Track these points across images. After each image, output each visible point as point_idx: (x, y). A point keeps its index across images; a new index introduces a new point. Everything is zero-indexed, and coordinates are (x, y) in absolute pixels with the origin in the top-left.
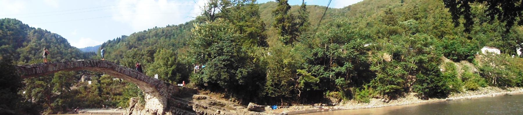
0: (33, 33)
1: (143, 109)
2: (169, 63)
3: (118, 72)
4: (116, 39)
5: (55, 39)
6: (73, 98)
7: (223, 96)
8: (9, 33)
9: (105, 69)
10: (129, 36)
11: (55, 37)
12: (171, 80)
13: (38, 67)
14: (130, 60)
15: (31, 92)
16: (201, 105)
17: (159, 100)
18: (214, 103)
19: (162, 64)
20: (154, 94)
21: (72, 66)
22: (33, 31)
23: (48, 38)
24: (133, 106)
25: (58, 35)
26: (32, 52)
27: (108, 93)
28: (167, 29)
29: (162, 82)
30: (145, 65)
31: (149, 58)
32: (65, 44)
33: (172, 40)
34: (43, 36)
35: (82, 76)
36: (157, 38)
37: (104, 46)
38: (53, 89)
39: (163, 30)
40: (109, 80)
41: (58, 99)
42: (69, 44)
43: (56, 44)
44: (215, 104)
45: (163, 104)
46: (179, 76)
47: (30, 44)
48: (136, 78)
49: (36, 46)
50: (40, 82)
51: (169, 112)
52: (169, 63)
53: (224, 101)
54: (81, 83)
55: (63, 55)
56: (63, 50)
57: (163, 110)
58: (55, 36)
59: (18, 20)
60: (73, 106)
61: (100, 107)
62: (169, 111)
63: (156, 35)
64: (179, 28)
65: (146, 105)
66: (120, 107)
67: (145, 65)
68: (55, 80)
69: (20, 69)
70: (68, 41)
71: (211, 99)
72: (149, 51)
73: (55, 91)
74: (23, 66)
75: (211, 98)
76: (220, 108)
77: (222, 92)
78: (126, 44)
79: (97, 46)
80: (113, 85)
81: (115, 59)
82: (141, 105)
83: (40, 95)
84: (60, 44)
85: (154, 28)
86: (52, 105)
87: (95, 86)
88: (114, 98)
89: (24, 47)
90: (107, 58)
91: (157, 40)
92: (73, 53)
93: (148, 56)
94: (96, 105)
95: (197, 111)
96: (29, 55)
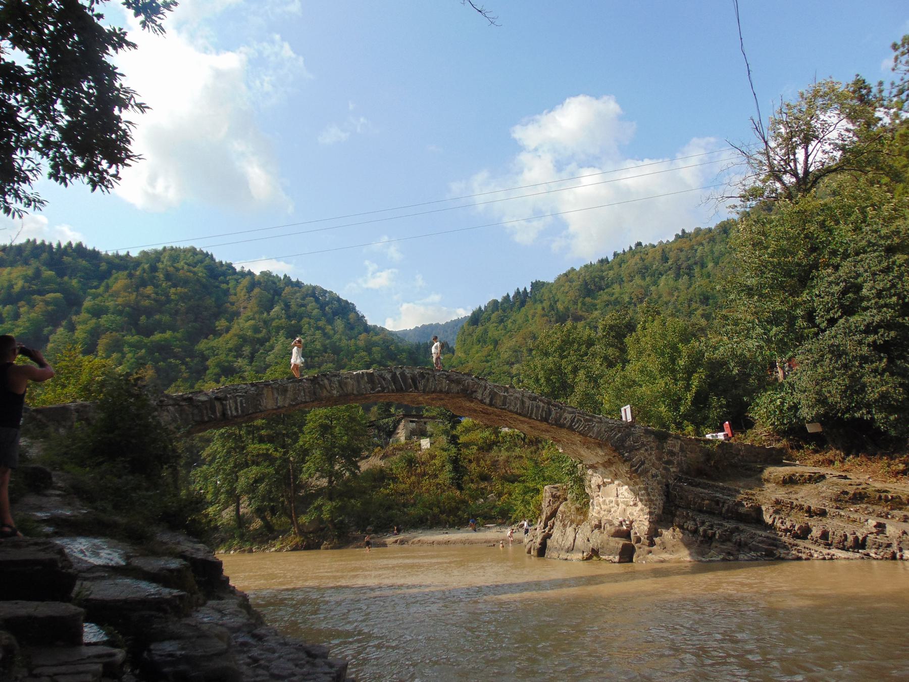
0: (245, 290)
1: (583, 521)
4: (511, 297)
7: (901, 467)
8: (175, 294)
10: (551, 280)
11: (317, 300)
12: (693, 423)
14: (550, 362)
16: (795, 503)
17: (631, 490)
18: (855, 494)
20: (613, 469)
21: (335, 392)
22: (245, 282)
24: (553, 514)
26: (244, 349)
27: (484, 478)
28: (679, 244)
31: (611, 351)
32: (348, 320)
33: (700, 283)
34: (276, 297)
35: (399, 422)
36: (648, 279)
37: (476, 319)
38: (304, 469)
41: (319, 501)
42: (360, 319)
44: (859, 497)
45: (649, 502)
46: (721, 407)
48: (545, 420)
49: (256, 330)
50: (263, 446)
51: (671, 529)
55: (341, 356)
56: (340, 339)
58: (315, 294)
60: (369, 524)
61: (460, 523)
62: (673, 526)
63: (643, 271)
64: (718, 238)
69: (178, 405)
70: (357, 309)
72: (612, 327)
73: (310, 476)
74: (186, 396)
75: (845, 478)
76: (888, 514)
77: (893, 453)
78: (543, 309)
80: (500, 451)
81: (513, 364)
82: (578, 509)
83: (262, 487)
85: (634, 248)
86: (304, 519)
88: (505, 490)
89: (220, 335)
90: (487, 361)
92: (374, 349)
94: (444, 516)
95: (778, 524)
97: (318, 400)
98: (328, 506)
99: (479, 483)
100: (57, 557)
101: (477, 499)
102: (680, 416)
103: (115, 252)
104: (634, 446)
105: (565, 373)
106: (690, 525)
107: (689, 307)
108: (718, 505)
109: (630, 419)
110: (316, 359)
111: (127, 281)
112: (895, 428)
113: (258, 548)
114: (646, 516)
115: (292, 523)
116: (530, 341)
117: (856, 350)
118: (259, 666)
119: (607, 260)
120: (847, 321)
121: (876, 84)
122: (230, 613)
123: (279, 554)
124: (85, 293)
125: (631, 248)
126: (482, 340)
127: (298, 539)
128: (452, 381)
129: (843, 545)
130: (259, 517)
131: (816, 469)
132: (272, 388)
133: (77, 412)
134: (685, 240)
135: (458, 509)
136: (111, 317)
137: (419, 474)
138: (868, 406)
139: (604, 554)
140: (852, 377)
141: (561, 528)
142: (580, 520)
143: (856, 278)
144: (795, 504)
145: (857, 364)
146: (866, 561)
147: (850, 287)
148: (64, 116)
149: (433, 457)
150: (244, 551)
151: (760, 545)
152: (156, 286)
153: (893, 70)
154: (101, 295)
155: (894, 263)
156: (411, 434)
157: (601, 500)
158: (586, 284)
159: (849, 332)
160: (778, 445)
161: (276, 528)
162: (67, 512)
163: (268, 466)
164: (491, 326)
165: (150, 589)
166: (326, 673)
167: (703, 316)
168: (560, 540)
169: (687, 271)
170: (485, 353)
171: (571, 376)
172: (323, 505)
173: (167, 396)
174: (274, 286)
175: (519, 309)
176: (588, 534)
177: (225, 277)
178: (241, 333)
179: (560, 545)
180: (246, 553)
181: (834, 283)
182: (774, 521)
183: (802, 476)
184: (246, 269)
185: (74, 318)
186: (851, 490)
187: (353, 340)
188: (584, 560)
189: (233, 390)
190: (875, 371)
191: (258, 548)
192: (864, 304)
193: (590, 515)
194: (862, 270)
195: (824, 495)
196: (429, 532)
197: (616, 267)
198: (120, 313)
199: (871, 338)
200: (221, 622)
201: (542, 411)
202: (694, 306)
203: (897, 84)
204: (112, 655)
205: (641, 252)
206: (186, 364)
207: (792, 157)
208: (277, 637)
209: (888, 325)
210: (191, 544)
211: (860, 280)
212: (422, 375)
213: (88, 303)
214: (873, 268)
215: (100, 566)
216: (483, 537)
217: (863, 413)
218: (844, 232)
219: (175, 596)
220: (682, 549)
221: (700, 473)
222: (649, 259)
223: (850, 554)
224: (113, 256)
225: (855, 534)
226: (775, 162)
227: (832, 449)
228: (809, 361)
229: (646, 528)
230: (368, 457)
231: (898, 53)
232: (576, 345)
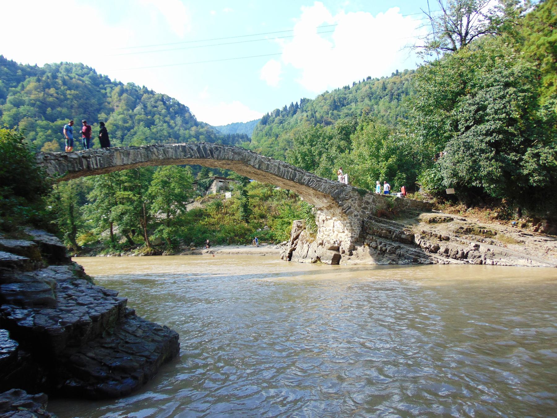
0: (117, 94)
2: (382, 151)
3: (255, 168)
4: (288, 108)
5: (163, 106)
7: (496, 215)
8: (70, 95)
9: (230, 162)
14: (305, 149)
16: (433, 233)
18: (467, 229)
19: (366, 154)
20: (332, 210)
22: (117, 89)
23: (149, 105)
24: (297, 237)
26: (117, 133)
27: (263, 216)
28: (393, 79)
30: (336, 158)
32: (184, 117)
34: (138, 100)
35: (212, 181)
36: (373, 101)
37: (265, 121)
38: (152, 208)
39: (384, 83)
40: (265, 190)
41: (161, 227)
42: (192, 117)
43: (166, 116)
44: (469, 231)
47: (113, 117)
48: (292, 180)
50: (126, 193)
52: (382, 151)
53: (496, 226)
54: (210, 196)
56: (179, 130)
58: (164, 100)
65: (319, 233)
69: (57, 159)
70: (190, 110)
72: (343, 129)
73: (156, 212)
75: (465, 220)
77: (493, 207)
78: (307, 116)
79: (253, 122)
80: (273, 201)
82: (311, 234)
83: (126, 218)
84: (173, 118)
86: (152, 238)
90: (271, 147)
91: (372, 105)
92: (201, 137)
95: (422, 245)
98: (167, 230)
101: (257, 229)
108: (390, 233)
112: (495, 192)
115: (145, 240)
123: (137, 257)
124: (8, 90)
125: (364, 80)
126: (268, 134)
134: (397, 77)
135: (246, 234)
136: (26, 107)
137: (223, 213)
138: (481, 179)
139: (323, 259)
140: (474, 161)
143: (484, 102)
145: (478, 154)
146: (466, 265)
150: (116, 255)
152: (57, 89)
154: (19, 92)
155: (507, 93)
156: (220, 189)
158: (335, 102)
159: (476, 134)
160: (431, 202)
161: (136, 242)
164: (274, 125)
166: (112, 304)
168: (300, 252)
169: (397, 97)
170: (270, 142)
171: (317, 157)
172: (163, 229)
174: (136, 93)
175: (293, 115)
176: (316, 248)
177: (104, 85)
178: (115, 122)
180: (117, 256)
186: (465, 227)
188: (312, 262)
190: (487, 158)
192: (487, 118)
196: (228, 247)
197: (354, 92)
198: (33, 105)
199: (488, 139)
207: (459, 22)
209: (499, 131)
210: (48, 237)
211: (486, 103)
212: (217, 149)
213: (10, 98)
214: (495, 96)
218: (481, 74)
222: (374, 88)
223: (459, 261)
224: (26, 66)
230: (192, 202)
232: (321, 138)
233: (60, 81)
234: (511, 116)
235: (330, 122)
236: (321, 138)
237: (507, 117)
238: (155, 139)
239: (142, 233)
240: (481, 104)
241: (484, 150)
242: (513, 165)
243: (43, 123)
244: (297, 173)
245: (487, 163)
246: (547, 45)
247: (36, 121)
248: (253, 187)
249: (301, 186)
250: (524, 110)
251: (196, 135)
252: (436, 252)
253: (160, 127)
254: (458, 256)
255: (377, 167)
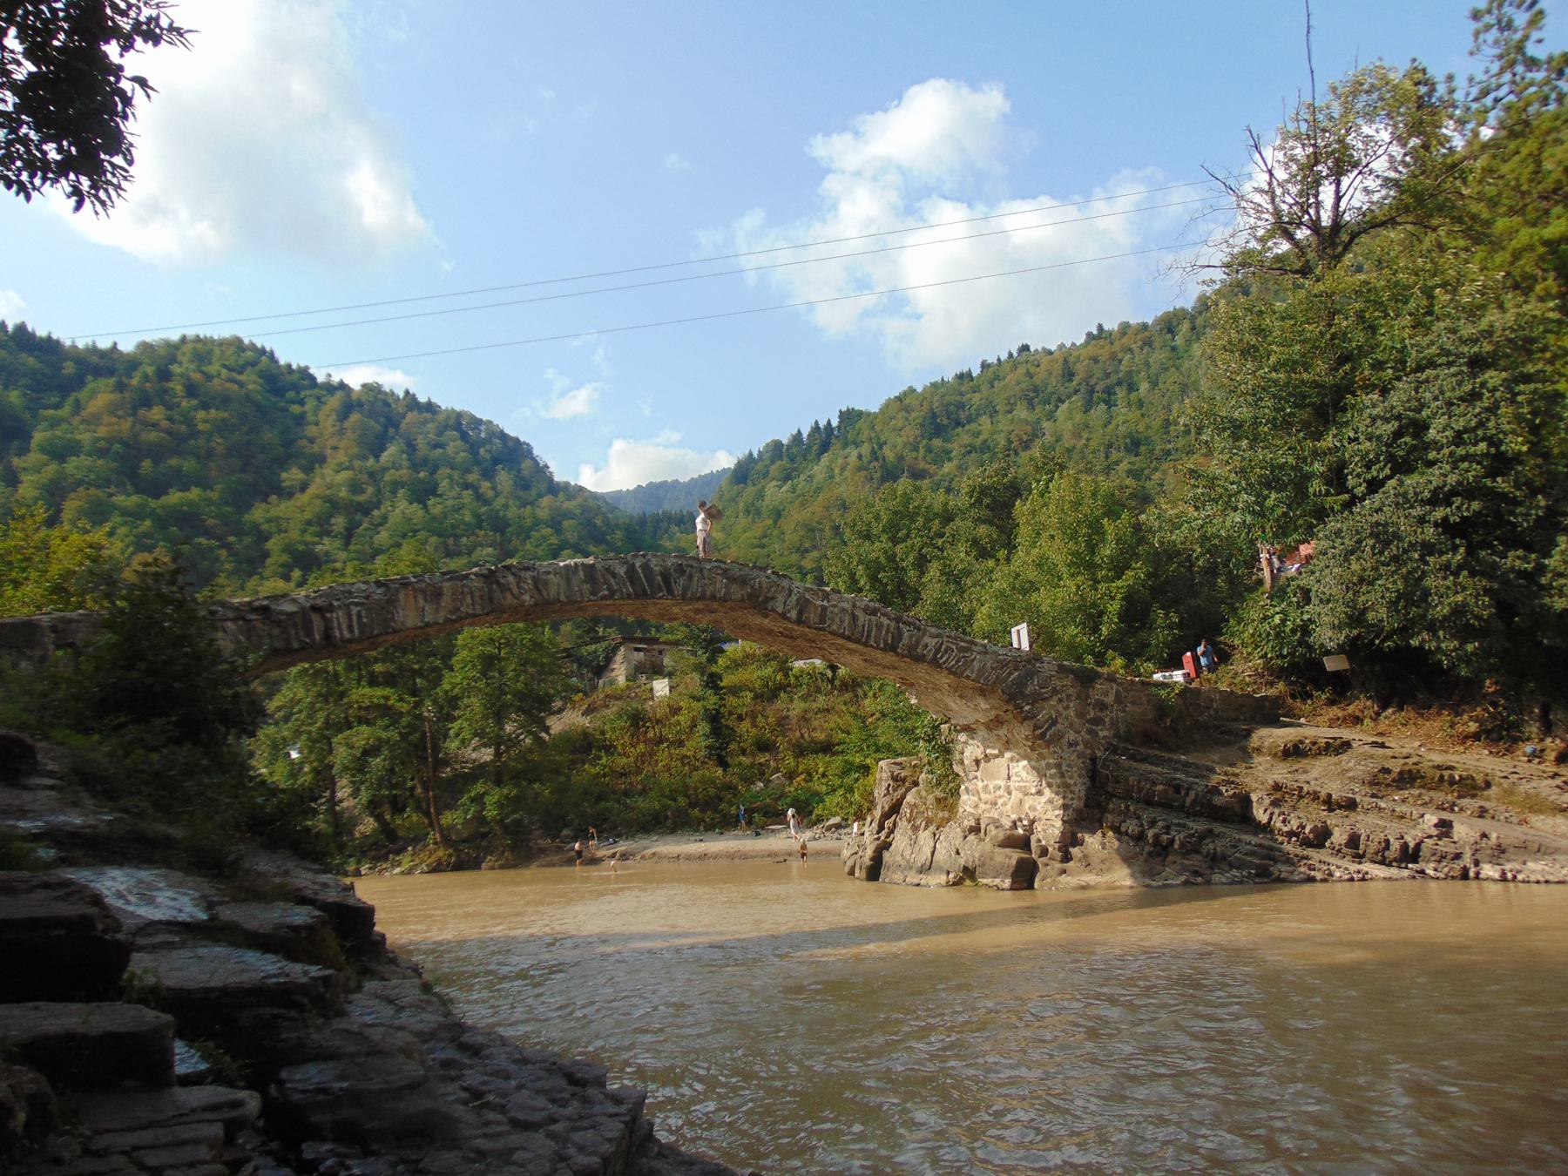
0: (334, 417)
2: (1107, 551)
3: (789, 619)
4: (805, 435)
5: (459, 442)
6: (568, 778)
7: (1473, 727)
8: (206, 421)
10: (874, 408)
11: (464, 436)
12: (1123, 654)
13: (336, 603)
15: (330, 751)
17: (1033, 768)
18: (1401, 773)
20: (1003, 732)
21: (527, 597)
22: (334, 402)
23: (421, 442)
24: (895, 808)
25: (480, 421)
26: (333, 521)
27: (765, 746)
28: (1091, 351)
29: (1048, 665)
30: (968, 573)
31: (983, 530)
32: (519, 471)
34: (391, 431)
35: (615, 650)
36: (1038, 409)
37: (744, 473)
38: (452, 732)
40: (768, 671)
41: (479, 788)
42: (541, 471)
44: (1408, 778)
45: (1064, 789)
46: (1170, 627)
49: (355, 487)
50: (380, 692)
51: (1099, 833)
52: (1107, 551)
53: (1478, 760)
54: (608, 691)
56: (506, 506)
57: (1064, 822)
58: (461, 424)
59: (253, 347)
60: (566, 826)
61: (726, 824)
63: (1032, 394)
66: (836, 820)
67: (968, 573)
68: (458, 680)
69: (243, 619)
70: (536, 452)
71: (1381, 751)
72: (984, 491)
75: (1382, 746)
76: (1454, 804)
77: (1459, 705)
78: (860, 457)
80: (792, 700)
81: (807, 551)
82: (938, 800)
83: (377, 762)
85: (1015, 355)
86: (448, 818)
87: (690, 709)
88: (801, 768)
89: (290, 495)
90: (763, 546)
91: (1038, 422)
92: (566, 523)
93: (979, 521)
95: (1277, 823)
96: (314, 544)
97: (493, 610)
98: (494, 796)
99: (754, 756)
100: (93, 911)
101: (753, 783)
102: (1101, 641)
103: (90, 343)
104: (1040, 694)
105: (903, 568)
106: (1131, 826)
107: (1107, 457)
109: (1025, 646)
110: (464, 540)
111: (116, 397)
113: (370, 868)
114: (1057, 812)
115: (431, 825)
116: (835, 514)
117: (1415, 532)
118: (486, 1105)
119: (969, 374)
120: (1401, 483)
121: (1443, 79)
122: (411, 1006)
123: (409, 879)
125: (1011, 355)
127: (440, 853)
128: (732, 580)
129: (1383, 856)
130: (372, 814)
131: (1334, 732)
132: (414, 590)
133: (53, 631)
134: (1102, 342)
135: (721, 799)
137: (650, 740)
139: (985, 875)
141: (910, 832)
142: (943, 819)
143: (1419, 411)
144: (1305, 790)
145: (1416, 556)
147: (1408, 426)
148: (23, 61)
149: (676, 710)
151: (1249, 859)
152: (169, 407)
153: (1472, 53)
155: (1483, 385)
156: (637, 671)
157: (980, 784)
158: (934, 416)
160: (1272, 692)
161: (401, 833)
162: (76, 820)
163: (387, 727)
165: (264, 967)
166: (612, 1116)
167: (1129, 473)
169: (1105, 396)
170: (759, 533)
173: (223, 604)
175: (819, 457)
176: (958, 842)
177: (298, 393)
178: (328, 492)
179: (908, 862)
181: (1382, 418)
182: (1270, 819)
183: (1314, 743)
184: (336, 379)
185: (16, 461)
186: (1396, 765)
187: (529, 507)
188: (948, 885)
189: (344, 592)
191: (370, 868)
192: (1432, 455)
193: (961, 810)
194: (1428, 395)
195: (1351, 774)
196: (670, 838)
197: (985, 388)
198: (103, 453)
199: (1439, 513)
200: (396, 1022)
201: (887, 632)
202: (1115, 456)
203: (1477, 80)
204: (236, 1104)
205: (1027, 362)
206: (228, 546)
208: (508, 1049)
209: (1468, 492)
210: (310, 875)
213: (39, 436)
214: (1448, 394)
215: (160, 922)
216: (765, 847)
217: (1423, 640)
218: (1397, 331)
219: (314, 979)
220: (1117, 867)
221: (1149, 739)
223: (1393, 872)
225: (1402, 838)
226: (1285, 207)
227: (1358, 698)
228: (1337, 551)
229: (1057, 832)
230: (560, 711)
231: (1479, 25)
232: (920, 521)
233: (178, 387)
234: (1503, 448)
235: (924, 470)
236: (920, 521)
237: (1493, 450)
238: (439, 535)
239: (424, 805)
240: (1408, 417)
241: (1433, 545)
242: (1520, 586)
243: (132, 501)
244: (905, 628)
245: (1447, 583)
246: (1541, 250)
247: (111, 495)
248: (735, 661)
249: (914, 666)
250: (1535, 430)
251: (553, 518)
252: (1321, 845)
253: (450, 498)
254: (1391, 854)
255: (1091, 596)
